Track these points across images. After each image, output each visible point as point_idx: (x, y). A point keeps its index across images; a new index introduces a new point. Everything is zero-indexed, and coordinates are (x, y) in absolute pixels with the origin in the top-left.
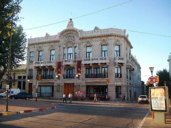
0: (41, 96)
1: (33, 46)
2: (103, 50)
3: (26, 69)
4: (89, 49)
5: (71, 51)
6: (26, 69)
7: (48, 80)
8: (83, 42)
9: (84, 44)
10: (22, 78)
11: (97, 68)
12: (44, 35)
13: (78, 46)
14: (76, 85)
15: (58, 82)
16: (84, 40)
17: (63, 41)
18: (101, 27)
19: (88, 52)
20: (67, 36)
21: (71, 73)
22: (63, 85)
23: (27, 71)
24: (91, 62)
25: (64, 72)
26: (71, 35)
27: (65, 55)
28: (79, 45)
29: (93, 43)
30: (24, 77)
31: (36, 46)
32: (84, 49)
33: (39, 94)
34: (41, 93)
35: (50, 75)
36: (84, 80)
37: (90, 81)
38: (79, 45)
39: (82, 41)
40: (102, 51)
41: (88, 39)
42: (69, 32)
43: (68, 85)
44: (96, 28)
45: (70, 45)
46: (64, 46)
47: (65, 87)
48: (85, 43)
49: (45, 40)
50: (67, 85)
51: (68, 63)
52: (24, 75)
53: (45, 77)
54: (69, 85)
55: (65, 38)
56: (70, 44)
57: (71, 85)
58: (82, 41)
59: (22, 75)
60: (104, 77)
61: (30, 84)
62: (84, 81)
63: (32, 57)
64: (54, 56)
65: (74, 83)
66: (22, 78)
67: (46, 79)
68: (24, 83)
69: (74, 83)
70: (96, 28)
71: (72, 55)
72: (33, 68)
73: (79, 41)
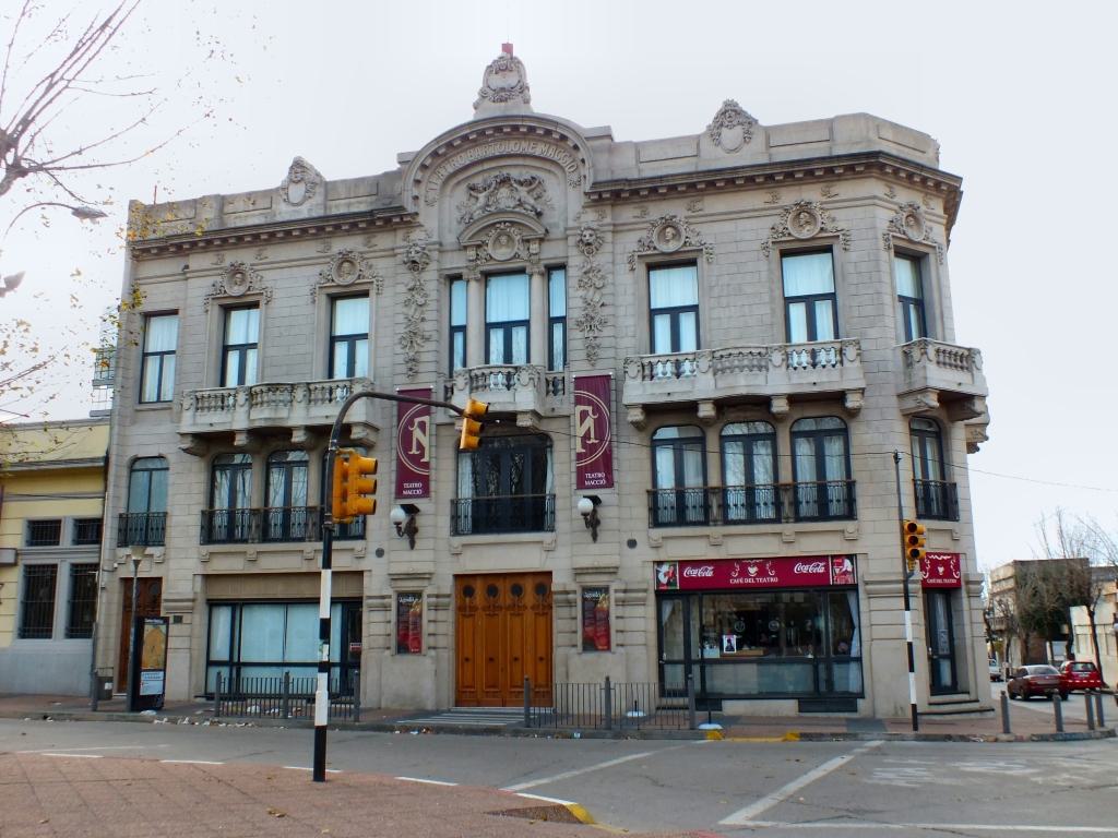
0: (230, 692)
1: (171, 266)
2: (234, 339)
3: (107, 453)
4: (673, 288)
5: (510, 300)
6: (107, 459)
7: (251, 548)
8: (616, 229)
9: (629, 242)
10: (67, 534)
11: (818, 437)
12: (274, 176)
13: (576, 261)
14: (567, 593)
15: (404, 559)
16: (628, 214)
17: (441, 216)
18: (767, 114)
19: (235, 347)
20: (478, 181)
21: (834, 471)
22: (447, 585)
23: (117, 472)
24: (238, 419)
25: (452, 481)
26: (514, 173)
27: (459, 338)
28: (588, 246)
29: (709, 233)
30: (88, 530)
31: (198, 261)
32: (625, 281)
33: (225, 671)
34: (235, 664)
35: (263, 514)
36: (642, 547)
37: (695, 546)
38: (588, 246)
39: (608, 220)
40: (333, 339)
41: (653, 198)
42: (512, 147)
43: (492, 591)
44: (731, 114)
45: (502, 253)
46: (456, 262)
47: (464, 612)
48: (644, 234)
49: (717, 158)
50: (480, 597)
51: (497, 399)
52: (89, 509)
53: (276, 532)
54: (504, 587)
55: (461, 194)
56: (505, 243)
57: (517, 591)
58: (608, 220)
59: (67, 508)
60: (280, 540)
61: (500, 585)
62: (644, 553)
63: (162, 354)
64: (170, 361)
65: (549, 574)
66: (67, 534)
67: (286, 537)
68: (84, 579)
69: (549, 574)
70: (731, 114)
71: (519, 335)
72: (172, 449)
73: (590, 217)
